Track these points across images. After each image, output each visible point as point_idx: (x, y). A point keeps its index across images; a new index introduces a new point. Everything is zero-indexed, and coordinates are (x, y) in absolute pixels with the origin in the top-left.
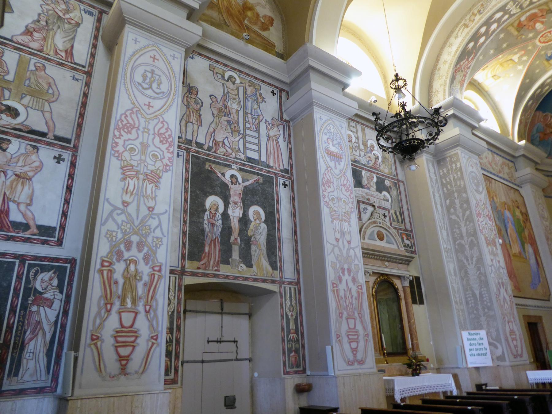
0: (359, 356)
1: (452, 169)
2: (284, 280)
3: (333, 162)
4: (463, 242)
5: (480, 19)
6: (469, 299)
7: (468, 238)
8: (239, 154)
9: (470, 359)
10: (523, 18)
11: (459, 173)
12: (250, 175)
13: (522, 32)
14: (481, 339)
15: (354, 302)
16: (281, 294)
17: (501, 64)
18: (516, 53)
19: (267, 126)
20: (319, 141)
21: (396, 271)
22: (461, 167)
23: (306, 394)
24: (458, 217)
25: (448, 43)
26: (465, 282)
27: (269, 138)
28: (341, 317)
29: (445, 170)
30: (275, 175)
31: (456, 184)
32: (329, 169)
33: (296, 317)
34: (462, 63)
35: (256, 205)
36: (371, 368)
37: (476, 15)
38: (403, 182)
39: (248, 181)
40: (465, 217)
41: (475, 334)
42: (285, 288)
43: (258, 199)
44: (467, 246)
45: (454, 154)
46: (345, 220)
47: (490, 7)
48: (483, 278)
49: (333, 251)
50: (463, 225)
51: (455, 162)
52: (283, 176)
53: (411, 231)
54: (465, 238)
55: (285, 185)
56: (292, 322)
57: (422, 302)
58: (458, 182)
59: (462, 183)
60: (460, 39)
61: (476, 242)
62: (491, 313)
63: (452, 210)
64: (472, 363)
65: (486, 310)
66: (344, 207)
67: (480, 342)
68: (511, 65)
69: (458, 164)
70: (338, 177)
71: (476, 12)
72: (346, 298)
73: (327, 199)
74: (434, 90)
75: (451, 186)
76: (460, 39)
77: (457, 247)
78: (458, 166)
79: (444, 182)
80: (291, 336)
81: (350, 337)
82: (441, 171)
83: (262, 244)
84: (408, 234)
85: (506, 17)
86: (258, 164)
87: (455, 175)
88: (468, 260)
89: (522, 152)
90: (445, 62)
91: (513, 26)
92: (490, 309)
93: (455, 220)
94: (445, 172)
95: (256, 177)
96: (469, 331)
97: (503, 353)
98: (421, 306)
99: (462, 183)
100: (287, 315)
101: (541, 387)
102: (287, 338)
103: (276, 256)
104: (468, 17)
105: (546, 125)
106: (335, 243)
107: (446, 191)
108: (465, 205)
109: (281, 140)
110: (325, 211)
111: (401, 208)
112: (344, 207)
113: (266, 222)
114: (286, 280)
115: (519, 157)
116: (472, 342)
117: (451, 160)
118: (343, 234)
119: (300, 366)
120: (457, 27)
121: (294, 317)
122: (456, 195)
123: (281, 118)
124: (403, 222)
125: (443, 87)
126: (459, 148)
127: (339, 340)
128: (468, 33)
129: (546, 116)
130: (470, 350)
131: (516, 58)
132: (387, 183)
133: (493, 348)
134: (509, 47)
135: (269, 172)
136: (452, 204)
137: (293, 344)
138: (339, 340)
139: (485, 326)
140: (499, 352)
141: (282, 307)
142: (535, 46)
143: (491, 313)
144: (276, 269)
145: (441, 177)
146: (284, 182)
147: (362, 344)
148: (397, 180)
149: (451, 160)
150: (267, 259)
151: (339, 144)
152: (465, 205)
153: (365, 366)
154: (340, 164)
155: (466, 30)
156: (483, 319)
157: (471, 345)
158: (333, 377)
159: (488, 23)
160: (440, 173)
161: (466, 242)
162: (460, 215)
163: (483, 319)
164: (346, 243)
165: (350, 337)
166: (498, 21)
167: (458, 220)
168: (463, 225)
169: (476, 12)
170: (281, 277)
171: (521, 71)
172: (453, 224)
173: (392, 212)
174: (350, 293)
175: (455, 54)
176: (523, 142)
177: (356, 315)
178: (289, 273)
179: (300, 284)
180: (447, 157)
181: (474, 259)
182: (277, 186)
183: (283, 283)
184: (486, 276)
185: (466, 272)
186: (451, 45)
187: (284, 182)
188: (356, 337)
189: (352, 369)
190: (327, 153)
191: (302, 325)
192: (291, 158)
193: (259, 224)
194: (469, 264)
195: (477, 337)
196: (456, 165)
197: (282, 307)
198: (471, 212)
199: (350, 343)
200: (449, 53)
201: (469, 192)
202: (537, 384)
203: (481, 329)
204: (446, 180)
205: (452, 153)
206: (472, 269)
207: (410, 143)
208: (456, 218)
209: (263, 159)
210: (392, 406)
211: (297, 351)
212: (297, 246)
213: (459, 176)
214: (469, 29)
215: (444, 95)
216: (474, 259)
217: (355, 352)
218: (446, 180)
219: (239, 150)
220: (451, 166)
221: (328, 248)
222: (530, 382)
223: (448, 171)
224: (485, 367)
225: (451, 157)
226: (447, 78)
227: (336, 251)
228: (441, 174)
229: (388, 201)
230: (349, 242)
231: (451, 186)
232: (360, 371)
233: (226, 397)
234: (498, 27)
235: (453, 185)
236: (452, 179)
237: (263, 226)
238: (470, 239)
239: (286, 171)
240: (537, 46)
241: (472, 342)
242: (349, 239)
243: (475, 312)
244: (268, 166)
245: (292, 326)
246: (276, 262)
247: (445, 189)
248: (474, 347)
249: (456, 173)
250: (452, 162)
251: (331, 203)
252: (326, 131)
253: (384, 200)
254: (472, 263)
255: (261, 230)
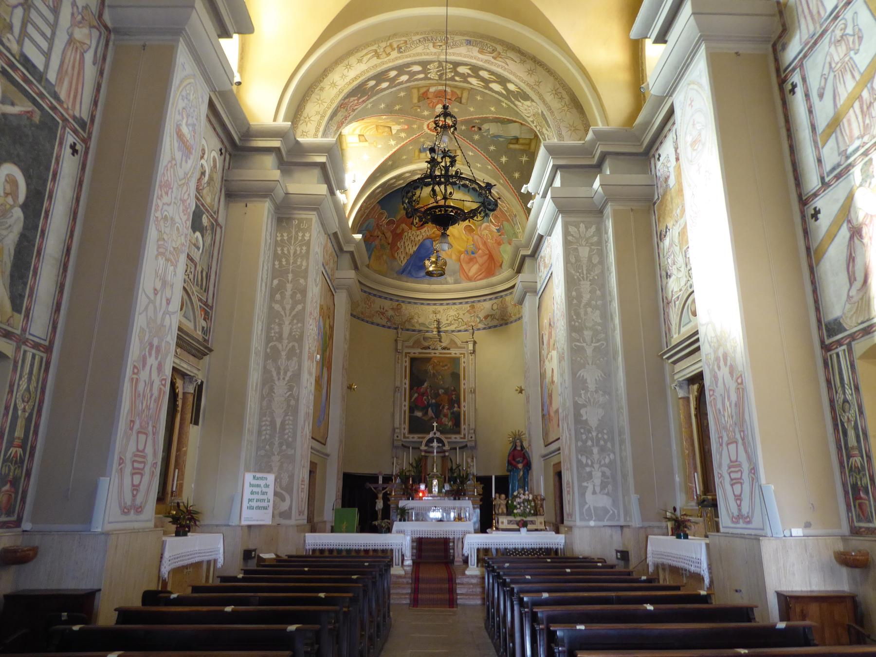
0: (139, 500)
1: (296, 238)
2: (27, 336)
3: (180, 153)
4: (280, 346)
5: (396, 59)
6: (264, 428)
7: (289, 343)
8: (10, 36)
9: (246, 513)
10: (432, 90)
11: (304, 248)
12: (20, 95)
13: (421, 104)
14: (267, 486)
15: (152, 406)
16: (16, 363)
17: (377, 126)
18: (399, 124)
19: (73, 14)
20: (173, 104)
21: (185, 366)
22: (309, 240)
23: (14, 568)
24: (284, 309)
25: (346, 62)
26: (265, 403)
27: (71, 41)
28: (131, 429)
29: (285, 235)
30: (63, 121)
31: (295, 262)
32: (174, 162)
33: (31, 414)
34: (352, 99)
35: (15, 163)
36: (147, 521)
37: (393, 49)
38: (221, 228)
39: (13, 104)
40: (294, 313)
41: (262, 478)
42: (25, 352)
43: (22, 153)
44: (283, 354)
45: (306, 219)
46: (172, 262)
47: (414, 52)
48: (293, 402)
49: (146, 309)
50: (287, 323)
51: (304, 231)
52: (75, 132)
53: (211, 308)
54: (285, 342)
55: (75, 151)
56: (21, 423)
57: (196, 423)
58: (299, 260)
59: (304, 263)
60: (363, 67)
61: (298, 351)
62: (290, 452)
63: (278, 297)
64: (247, 519)
65: (284, 447)
66: (175, 239)
67: (264, 490)
68: (385, 134)
69: (307, 235)
70: (180, 183)
71: (395, 46)
72: (144, 396)
73: (158, 214)
74: (305, 114)
75: (287, 261)
76: (363, 67)
77: (268, 350)
78: (306, 238)
79: (279, 252)
80: (13, 450)
81: (136, 465)
82: (279, 235)
83: (6, 252)
84: (207, 311)
85: (422, 76)
86: (39, 81)
87: (298, 249)
88: (278, 373)
89: (351, 248)
90: (333, 84)
91: (419, 91)
92: (290, 445)
93: (278, 312)
94: (285, 238)
95: (28, 107)
96: (254, 474)
97: (290, 508)
98: (195, 427)
99: (304, 263)
100: (15, 409)
101: (318, 554)
102: (5, 456)
103: (25, 284)
104: (383, 45)
105: (377, 225)
106: (152, 296)
107: (277, 266)
108: (299, 296)
109: (89, 57)
110: (152, 234)
111: (210, 267)
112: (175, 239)
113: (24, 207)
114: (31, 337)
115: (347, 252)
116: (255, 489)
117: (298, 226)
118: (164, 283)
119: (14, 512)
120: (365, 48)
121: (27, 414)
122: (290, 276)
123: (100, 15)
124: (206, 290)
125: (318, 117)
126: (315, 213)
127: (121, 469)
128: (376, 66)
129: (382, 214)
130: (250, 500)
131: (395, 128)
132: (205, 220)
133: (278, 499)
134: (401, 112)
135: (54, 108)
136: (281, 288)
137: (12, 468)
138: (121, 469)
139: (276, 469)
140: (285, 506)
141: (11, 391)
142: (420, 127)
143: (290, 452)
144: (20, 312)
145: (277, 244)
146: (75, 144)
147: (146, 478)
148: (216, 221)
149: (298, 226)
150: (8, 285)
151: (194, 125)
152: (299, 296)
153: (142, 517)
154: (186, 162)
155: (375, 61)
156: (276, 458)
157: (252, 493)
158: (102, 534)
159: (401, 69)
160: (277, 236)
161: (284, 347)
162: (288, 307)
163: (276, 458)
164: (164, 302)
165: (136, 465)
166: (412, 74)
167: (282, 313)
168: (287, 323)
169: (395, 46)
170: (24, 330)
171: (391, 147)
172: (273, 317)
173: (199, 269)
174: (151, 390)
175: (350, 83)
176: (358, 237)
177: (150, 428)
178: (39, 327)
179: (51, 352)
180: (294, 219)
181: (289, 374)
182: (61, 144)
183: (25, 342)
184: (297, 400)
185: (271, 389)
186: (349, 66)
187: (75, 144)
188: (141, 466)
189: (126, 522)
190: (177, 134)
191: (36, 433)
192: (96, 103)
193: (12, 207)
194: (279, 379)
195: (262, 483)
196: (303, 236)
197: (11, 391)
198: (304, 308)
199: (732, 485)
200: (343, 76)
201: (309, 279)
202: (314, 551)
203: (269, 472)
204: (282, 250)
205: (304, 216)
206: (280, 389)
207: (446, 211)
208: (280, 309)
209: (52, 76)
210: (219, 580)
211: (14, 483)
212: (65, 276)
213: (304, 251)
214: (379, 61)
215: (317, 130)
216: (289, 374)
217: (135, 492)
218: (282, 250)
219: (10, 27)
220: (297, 233)
221: (142, 301)
222: (308, 547)
223: (289, 239)
224: (260, 526)
225: (301, 221)
226: (329, 108)
227: (151, 312)
228: (279, 239)
229: (198, 248)
230: (168, 302)
231: (287, 261)
232: (137, 525)
233: (478, 550)
234: (407, 81)
235: (291, 261)
236: (292, 252)
237: (18, 214)
238: (291, 344)
239: (82, 124)
240: (423, 129)
241: (255, 489)
242: (169, 296)
243: (267, 447)
244: (56, 96)
245: (19, 433)
246: (22, 297)
247: (277, 263)
248: (255, 497)
249: (301, 246)
250: (298, 228)
251: (162, 223)
252: (184, 93)
253: (195, 245)
254: (284, 379)
255: (10, 221)
